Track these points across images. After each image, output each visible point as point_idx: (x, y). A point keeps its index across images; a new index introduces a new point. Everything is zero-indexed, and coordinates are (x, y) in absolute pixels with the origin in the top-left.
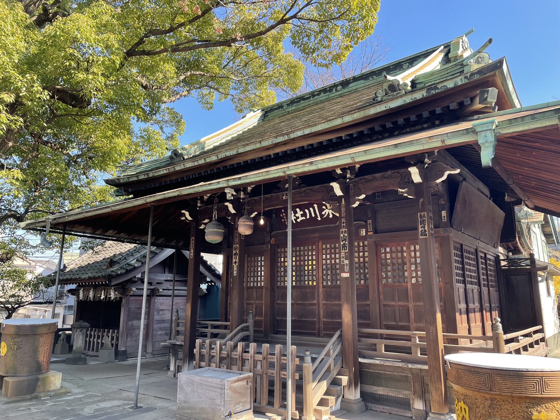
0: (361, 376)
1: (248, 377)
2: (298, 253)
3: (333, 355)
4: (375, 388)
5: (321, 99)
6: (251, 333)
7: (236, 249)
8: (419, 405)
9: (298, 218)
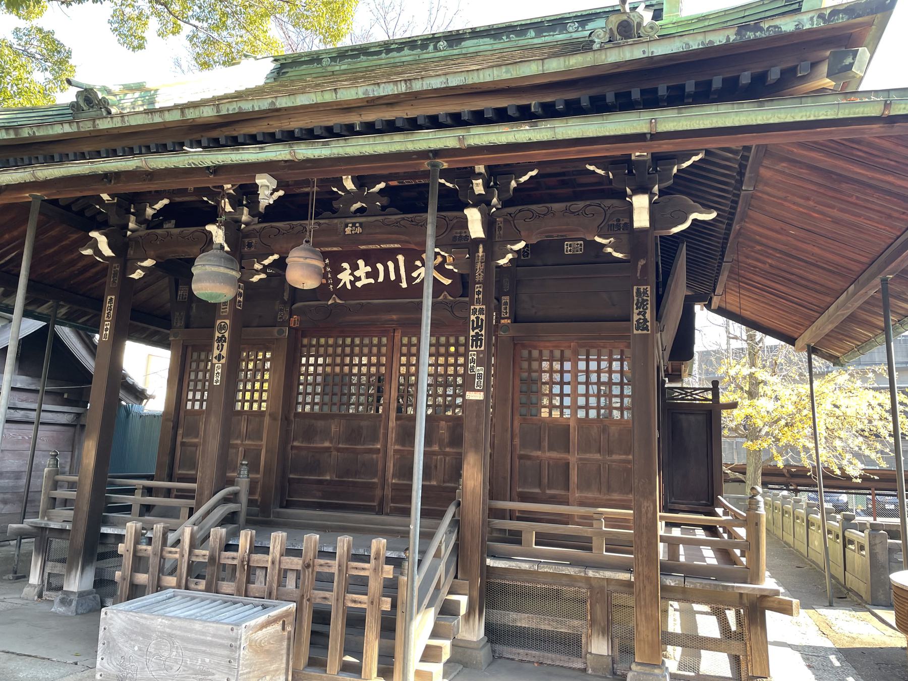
0: (491, 593)
1: (287, 614)
2: (375, 350)
3: (446, 553)
4: (513, 615)
5: (404, 59)
6: (242, 506)
7: (222, 328)
8: (599, 647)
9: (359, 279)
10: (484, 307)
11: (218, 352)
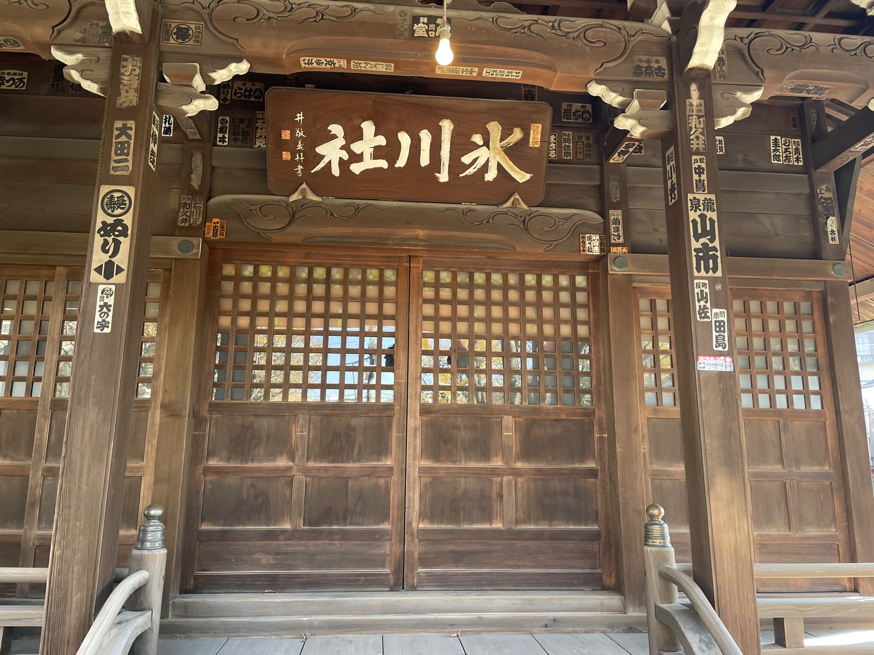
9: (359, 158)
10: (713, 197)
11: (106, 258)
